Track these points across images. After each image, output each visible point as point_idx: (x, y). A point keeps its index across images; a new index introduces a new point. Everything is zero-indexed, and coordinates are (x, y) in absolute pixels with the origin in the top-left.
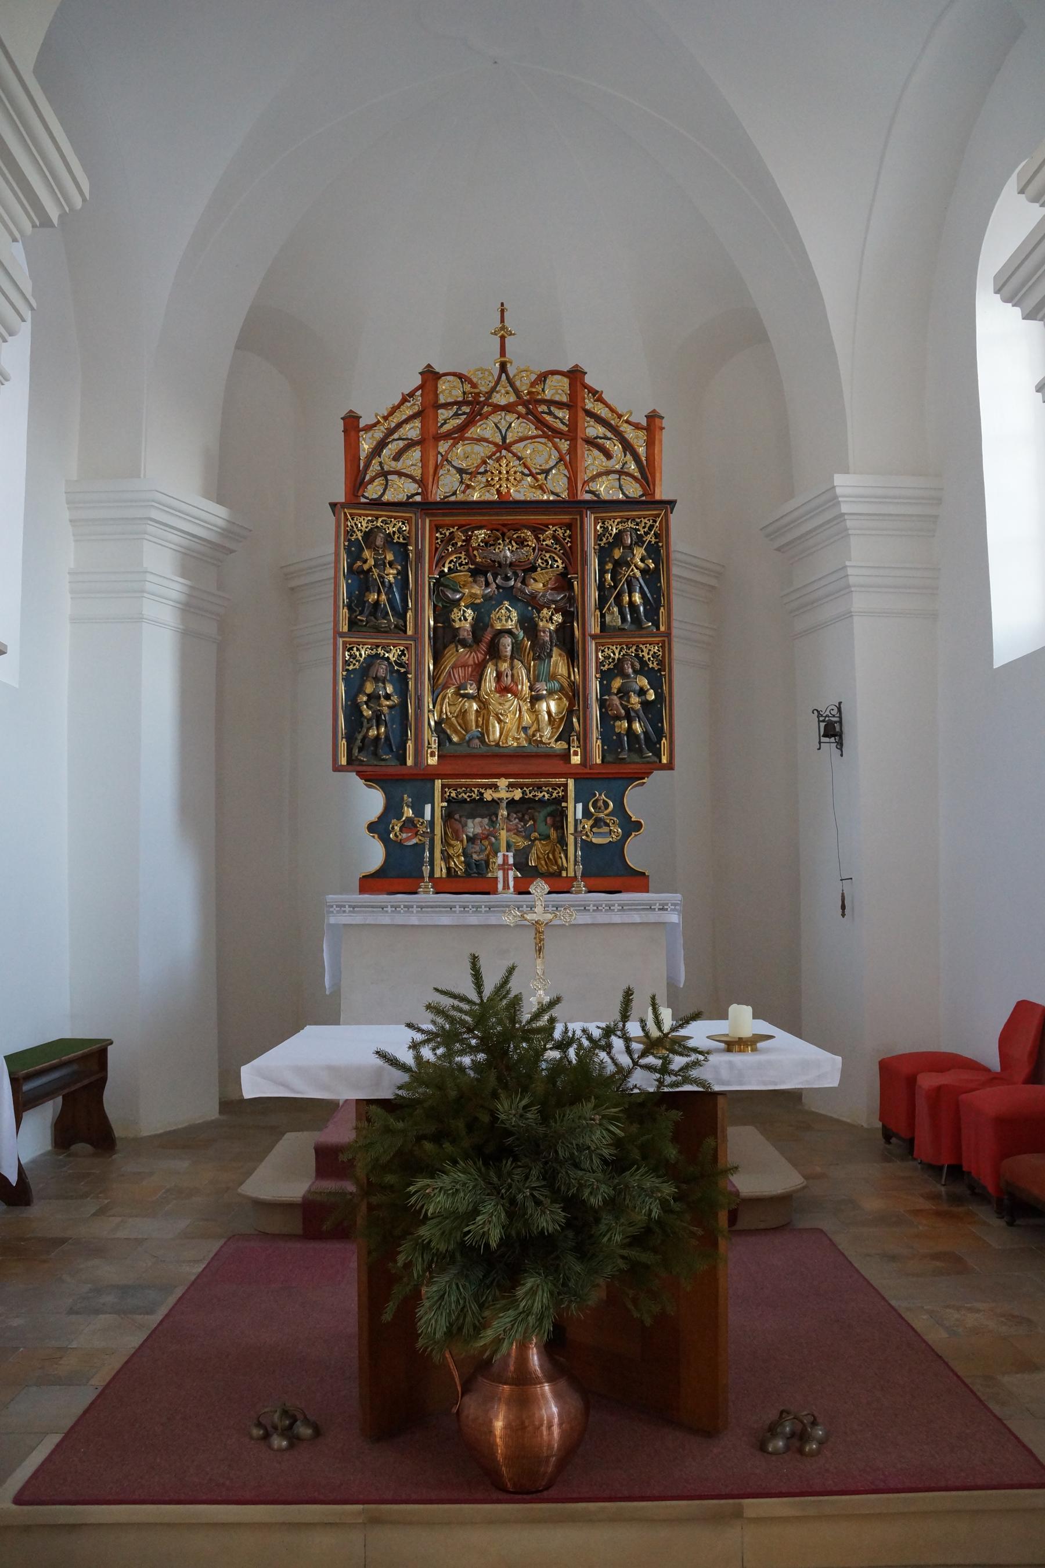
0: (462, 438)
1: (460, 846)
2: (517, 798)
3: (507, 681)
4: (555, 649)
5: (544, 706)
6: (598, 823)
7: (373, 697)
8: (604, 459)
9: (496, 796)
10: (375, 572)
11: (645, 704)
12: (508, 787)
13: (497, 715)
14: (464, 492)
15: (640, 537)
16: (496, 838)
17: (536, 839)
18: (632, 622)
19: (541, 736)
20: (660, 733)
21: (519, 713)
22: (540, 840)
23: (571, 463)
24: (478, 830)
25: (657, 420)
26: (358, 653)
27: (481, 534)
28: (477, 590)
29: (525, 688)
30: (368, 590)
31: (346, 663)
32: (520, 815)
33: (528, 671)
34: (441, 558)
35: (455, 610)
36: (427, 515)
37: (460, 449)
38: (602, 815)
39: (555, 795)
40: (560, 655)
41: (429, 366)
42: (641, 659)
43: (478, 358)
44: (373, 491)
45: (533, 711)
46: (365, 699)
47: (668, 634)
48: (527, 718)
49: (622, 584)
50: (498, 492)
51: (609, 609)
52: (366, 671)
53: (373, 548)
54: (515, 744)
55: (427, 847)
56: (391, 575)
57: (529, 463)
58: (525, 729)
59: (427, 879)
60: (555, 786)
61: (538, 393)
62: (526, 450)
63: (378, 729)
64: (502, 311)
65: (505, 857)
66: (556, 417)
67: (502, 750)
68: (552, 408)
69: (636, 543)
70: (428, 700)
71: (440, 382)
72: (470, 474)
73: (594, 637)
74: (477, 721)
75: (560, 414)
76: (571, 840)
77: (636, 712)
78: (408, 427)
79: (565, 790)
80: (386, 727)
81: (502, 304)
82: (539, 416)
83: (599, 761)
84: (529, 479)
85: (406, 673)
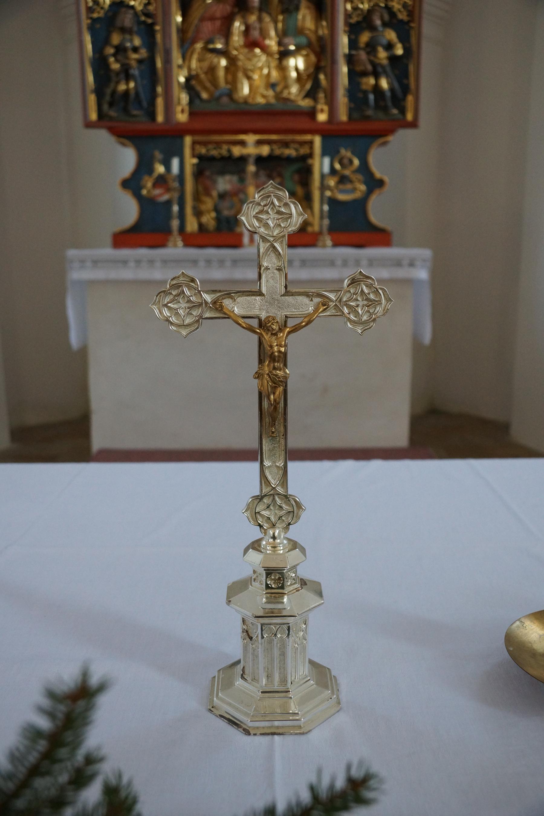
3: (255, 34)
5: (292, 62)
6: (343, 180)
7: (120, 50)
11: (393, 59)
20: (406, 90)
21: (270, 69)
29: (272, 43)
31: (90, 10)
40: (308, 8)
45: (282, 69)
48: (275, 74)
60: (302, 143)
77: (383, 67)
85: (153, 24)
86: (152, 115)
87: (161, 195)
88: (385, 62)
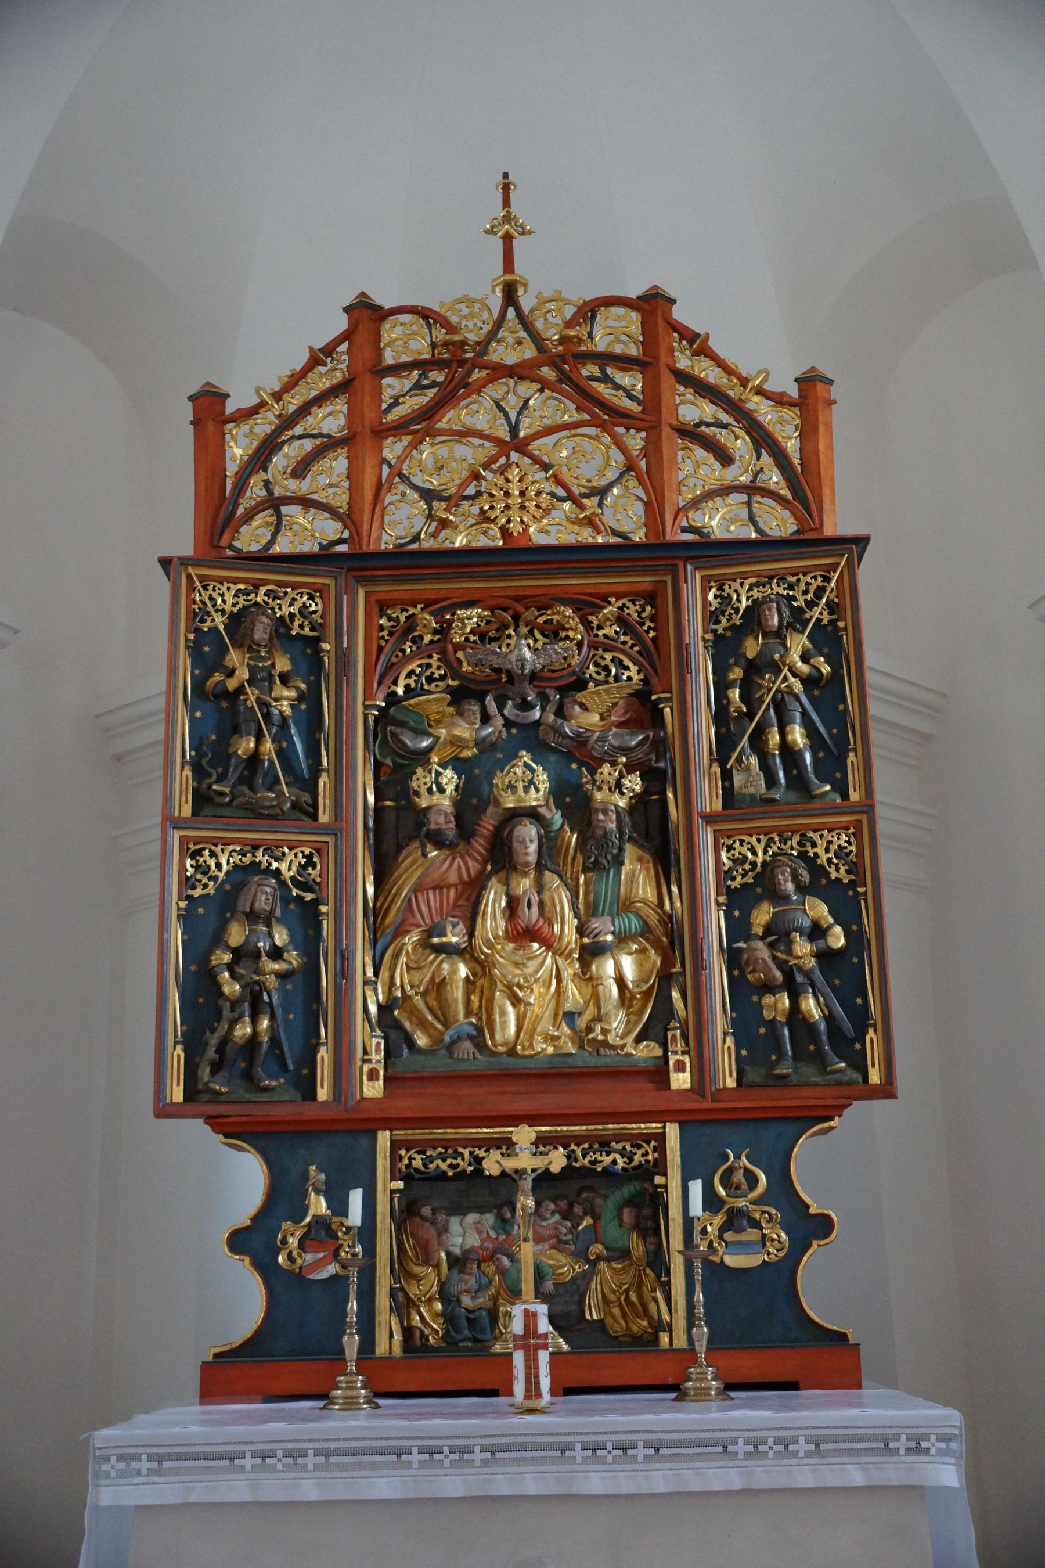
0: (431, 433)
1: (433, 1278)
2: (556, 1168)
3: (530, 915)
4: (629, 847)
5: (608, 967)
6: (735, 1220)
8: (717, 465)
9: (510, 1164)
10: (252, 695)
11: (826, 957)
12: (536, 1144)
13: (509, 987)
14: (434, 535)
17: (599, 1258)
18: (789, 785)
19: (605, 1032)
20: (861, 1019)
21: (557, 983)
22: (608, 1260)
23: (650, 474)
24: (473, 1240)
25: (820, 386)
26: (212, 863)
27: (472, 617)
28: (464, 730)
29: (567, 930)
31: (187, 883)
32: (563, 1204)
33: (575, 895)
34: (390, 666)
35: (420, 771)
36: (362, 581)
37: (426, 453)
38: (742, 1203)
39: (638, 1158)
40: (640, 860)
41: (363, 294)
42: (811, 863)
43: (461, 281)
44: (251, 537)
46: (227, 958)
47: (868, 808)
48: (574, 994)
49: (765, 707)
50: (505, 531)
51: (739, 760)
52: (229, 899)
53: (251, 648)
54: (550, 1050)
55: (353, 1289)
56: (284, 700)
57: (566, 477)
59: (352, 1367)
60: (639, 1140)
61: (581, 341)
62: (560, 451)
63: (254, 1022)
64: (506, 189)
65: (530, 1317)
66: (617, 387)
67: (522, 1063)
68: (609, 370)
69: (790, 625)
70: (362, 960)
71: (386, 326)
72: (448, 499)
73: (710, 819)
74: (468, 1003)
75: (625, 379)
76: (677, 1265)
78: (320, 413)
80: (273, 1017)
81: (506, 176)
82: (583, 384)
83: (731, 1083)
84: (567, 506)
85: (316, 903)
86: (311, 1094)
88: (811, 963)
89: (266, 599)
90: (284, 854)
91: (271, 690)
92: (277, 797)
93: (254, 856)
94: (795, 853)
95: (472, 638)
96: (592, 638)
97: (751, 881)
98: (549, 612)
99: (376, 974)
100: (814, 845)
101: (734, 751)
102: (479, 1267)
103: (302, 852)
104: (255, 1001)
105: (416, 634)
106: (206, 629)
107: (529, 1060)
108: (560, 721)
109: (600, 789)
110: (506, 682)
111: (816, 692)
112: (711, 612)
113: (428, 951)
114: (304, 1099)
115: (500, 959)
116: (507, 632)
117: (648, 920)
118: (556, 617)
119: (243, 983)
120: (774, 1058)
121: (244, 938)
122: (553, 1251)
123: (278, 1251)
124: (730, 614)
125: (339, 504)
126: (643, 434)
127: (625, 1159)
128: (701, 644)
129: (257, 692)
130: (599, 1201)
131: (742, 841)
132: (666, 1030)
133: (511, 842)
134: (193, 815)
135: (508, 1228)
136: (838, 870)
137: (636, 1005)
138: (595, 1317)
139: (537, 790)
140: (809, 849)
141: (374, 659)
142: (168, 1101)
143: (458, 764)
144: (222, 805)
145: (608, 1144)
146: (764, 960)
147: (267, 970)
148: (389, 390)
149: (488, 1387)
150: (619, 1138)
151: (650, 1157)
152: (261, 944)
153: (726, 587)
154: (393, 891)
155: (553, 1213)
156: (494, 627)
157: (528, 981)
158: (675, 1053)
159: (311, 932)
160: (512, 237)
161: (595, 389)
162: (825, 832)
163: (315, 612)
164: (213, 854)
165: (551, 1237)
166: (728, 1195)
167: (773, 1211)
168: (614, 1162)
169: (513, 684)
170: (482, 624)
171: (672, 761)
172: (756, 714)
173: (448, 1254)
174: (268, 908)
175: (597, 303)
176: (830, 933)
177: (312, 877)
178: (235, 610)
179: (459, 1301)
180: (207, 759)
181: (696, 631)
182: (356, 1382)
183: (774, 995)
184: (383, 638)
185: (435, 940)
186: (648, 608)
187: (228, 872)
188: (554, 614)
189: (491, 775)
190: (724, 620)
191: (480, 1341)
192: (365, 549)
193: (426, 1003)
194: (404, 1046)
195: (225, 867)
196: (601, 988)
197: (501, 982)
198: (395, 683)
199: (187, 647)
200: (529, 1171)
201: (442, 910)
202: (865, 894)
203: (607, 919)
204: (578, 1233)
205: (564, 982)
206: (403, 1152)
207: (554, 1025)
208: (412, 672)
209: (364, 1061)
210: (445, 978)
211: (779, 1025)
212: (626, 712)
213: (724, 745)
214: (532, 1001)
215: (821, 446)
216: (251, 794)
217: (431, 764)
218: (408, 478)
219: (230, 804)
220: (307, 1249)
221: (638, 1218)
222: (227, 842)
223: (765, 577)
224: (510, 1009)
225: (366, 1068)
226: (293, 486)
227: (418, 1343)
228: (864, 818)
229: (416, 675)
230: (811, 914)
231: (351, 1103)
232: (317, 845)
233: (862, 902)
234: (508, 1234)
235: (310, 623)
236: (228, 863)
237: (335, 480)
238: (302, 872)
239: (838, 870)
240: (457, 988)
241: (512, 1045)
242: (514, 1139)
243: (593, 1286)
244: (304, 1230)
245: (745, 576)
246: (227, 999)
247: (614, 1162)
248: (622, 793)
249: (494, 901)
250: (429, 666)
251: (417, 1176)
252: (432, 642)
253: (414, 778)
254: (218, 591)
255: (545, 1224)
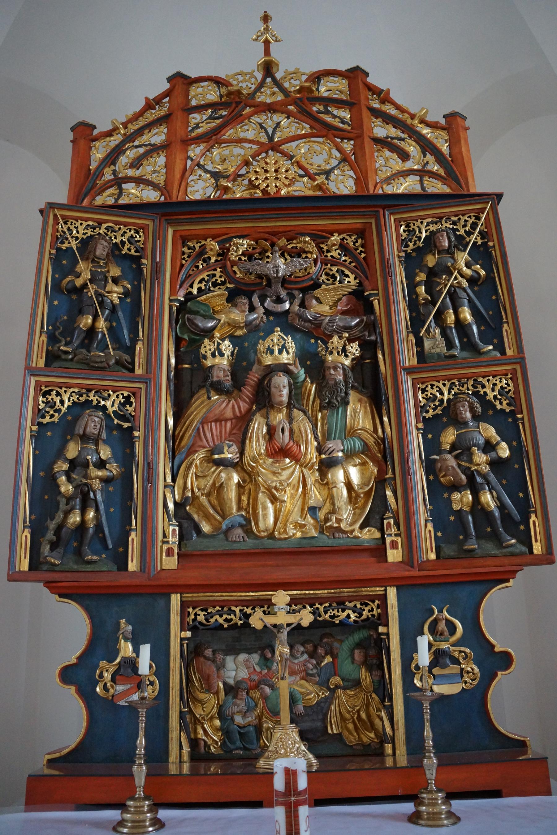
1: (213, 701)
4: (351, 393)
5: (339, 475)
8: (400, 161)
9: (270, 620)
10: (92, 290)
11: (496, 464)
13: (269, 489)
15: (460, 238)
16: (272, 687)
17: (337, 687)
20: (525, 509)
22: (344, 688)
24: (244, 674)
26: (58, 400)
27: (244, 244)
28: (237, 316)
30: (81, 312)
31: (39, 413)
32: (310, 647)
34: (188, 276)
35: (206, 341)
36: (170, 223)
38: (444, 646)
39: (365, 614)
40: (360, 401)
42: (482, 398)
45: (324, 482)
47: (521, 360)
48: (316, 496)
51: (428, 331)
52: (68, 427)
54: (299, 535)
57: (304, 162)
58: (313, 510)
59: (140, 793)
60: (365, 600)
62: (301, 149)
66: (335, 117)
67: (278, 544)
73: (409, 371)
74: (239, 501)
77: (484, 476)
79: (384, 604)
80: (97, 510)
83: (433, 556)
84: (305, 179)
85: (131, 429)
86: (122, 562)
87: (126, 693)
88: (486, 469)
89: (106, 231)
90: (109, 395)
91: (105, 286)
92: (105, 356)
93: (88, 396)
94: (470, 392)
95: (243, 258)
96: (323, 257)
97: (440, 412)
98: (294, 242)
99: (174, 480)
100: (483, 387)
101: (423, 328)
102: (248, 694)
103: (123, 394)
104: (85, 498)
105: (206, 256)
106: (64, 248)
107: (284, 542)
108: (302, 310)
109: (331, 353)
110: (266, 285)
111: (476, 288)
112: (402, 240)
113: (211, 465)
114: (119, 570)
115: (262, 470)
116: (267, 255)
117: (367, 442)
118: (299, 245)
119: (75, 484)
120: (461, 537)
121: (77, 453)
122: (303, 682)
123: (96, 683)
124: (415, 241)
125: (158, 182)
126: (352, 142)
127: (356, 614)
128: (397, 259)
129: (95, 287)
130: (336, 645)
131: (432, 386)
132: (383, 519)
133: (270, 387)
134: (45, 366)
135: (269, 664)
136: (501, 403)
137: (361, 502)
138: (335, 732)
139: (288, 353)
140: (480, 389)
141: (178, 270)
142: (17, 570)
143: (233, 338)
144: (66, 360)
145: (343, 603)
146: (452, 467)
147: (93, 475)
148: (193, 120)
149: (253, 799)
150: (351, 598)
151: (375, 612)
152: (89, 457)
153: (411, 225)
154: (187, 423)
155: (303, 653)
156: (258, 251)
157: (283, 485)
158: (391, 535)
159: (128, 451)
160: (269, 42)
161: (321, 117)
162: (491, 378)
163: (139, 241)
164: (58, 394)
165: (300, 672)
166: (435, 640)
167: (468, 651)
168: (348, 616)
169: (271, 287)
170: (250, 250)
171: (381, 334)
172: (438, 301)
173: (225, 684)
174: (96, 432)
175: (321, 73)
176: (498, 447)
177: (129, 412)
178: (85, 237)
179: (233, 720)
180: (59, 331)
181: (394, 252)
182: (143, 807)
183: (460, 493)
184: (184, 259)
185: (216, 457)
186: (360, 241)
187: (69, 406)
188: (298, 243)
189: (257, 344)
190: (411, 245)
191: (249, 750)
192: (174, 200)
193: (209, 502)
194: (194, 532)
195: (67, 404)
196: (335, 489)
197: (263, 486)
198: (191, 286)
199: (50, 258)
200: (285, 626)
201: (221, 436)
202: (522, 419)
203: (339, 441)
204: (321, 669)
205: (309, 486)
206: (190, 610)
207: (301, 517)
208: (203, 279)
209: (164, 542)
210: (223, 483)
211: (464, 513)
212: (347, 305)
213: (416, 323)
214: (285, 499)
215: (464, 149)
216: (87, 353)
217: (214, 338)
218: (203, 166)
219: (72, 360)
220: (117, 682)
221: (366, 656)
222: (69, 386)
223: (437, 218)
224: (270, 505)
225: (165, 547)
226: (131, 173)
227: (202, 750)
228: (518, 368)
229: (206, 282)
230: (485, 435)
231: (153, 573)
232: (133, 390)
233: (520, 424)
234: (269, 668)
235: (135, 247)
236: (69, 401)
237: (157, 168)
238: (122, 408)
239: (501, 403)
240: (231, 490)
241: (271, 531)
242: (273, 601)
243: (333, 707)
244: (115, 668)
245: (423, 218)
246: (64, 496)
247: (348, 616)
248: (347, 356)
249: (258, 428)
250: (214, 275)
251: (201, 627)
252: (216, 261)
253: (203, 346)
254: (74, 225)
255: (296, 661)
